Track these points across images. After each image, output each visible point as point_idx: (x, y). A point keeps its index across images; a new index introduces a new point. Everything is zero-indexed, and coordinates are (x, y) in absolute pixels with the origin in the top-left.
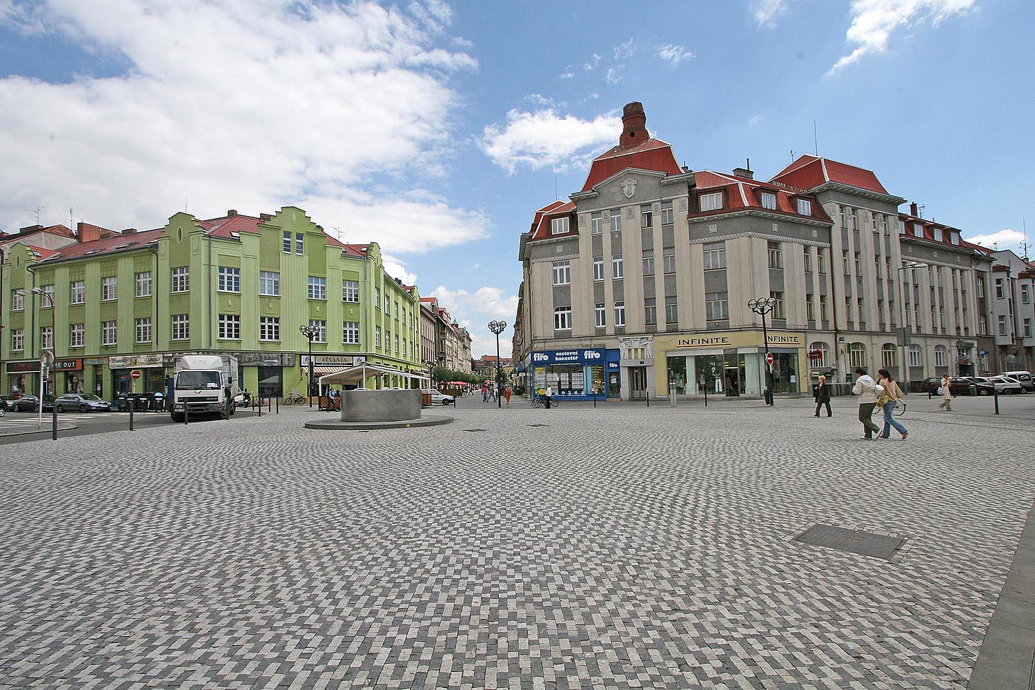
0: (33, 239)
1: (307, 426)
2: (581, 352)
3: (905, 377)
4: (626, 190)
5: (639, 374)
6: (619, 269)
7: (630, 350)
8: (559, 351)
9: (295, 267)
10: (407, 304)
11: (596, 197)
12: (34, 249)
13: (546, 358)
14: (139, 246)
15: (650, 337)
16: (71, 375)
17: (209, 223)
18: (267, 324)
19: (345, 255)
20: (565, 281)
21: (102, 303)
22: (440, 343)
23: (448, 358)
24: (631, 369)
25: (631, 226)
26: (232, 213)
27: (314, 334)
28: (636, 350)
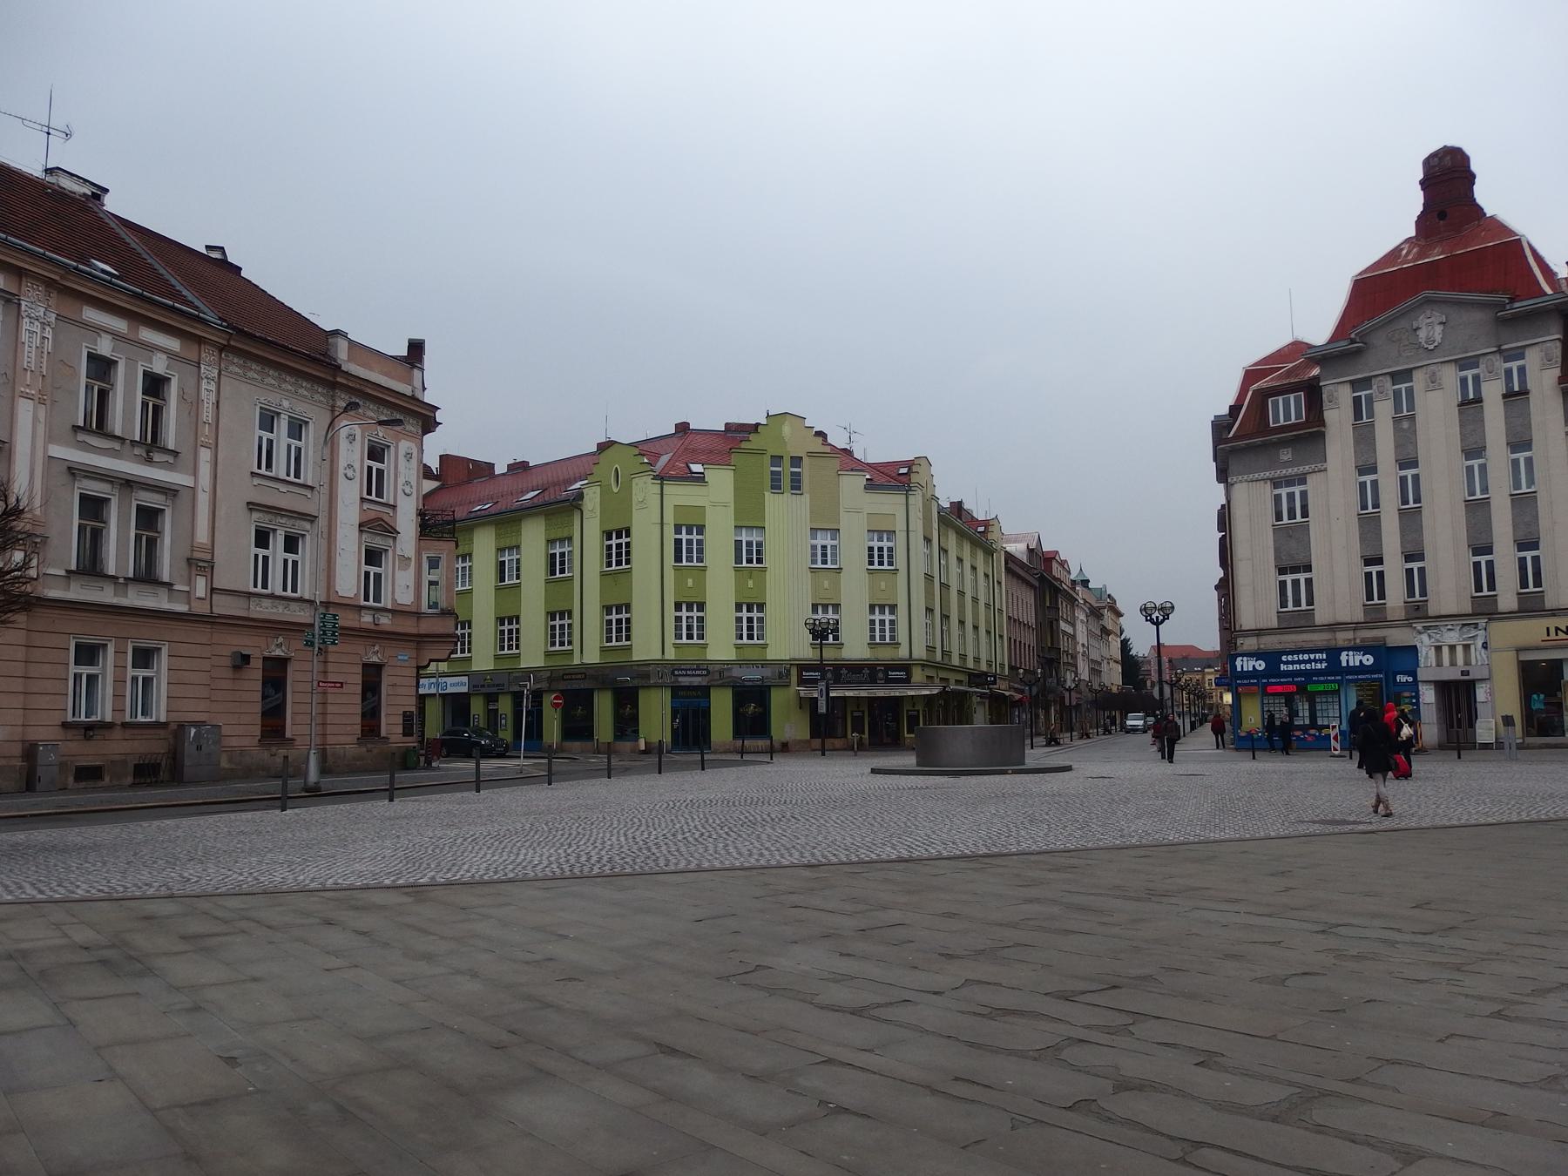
2: (1333, 653)
3: (751, 607)
4: (1422, 334)
5: (1458, 698)
6: (1410, 493)
7: (1438, 649)
8: (1287, 653)
9: (785, 518)
10: (980, 555)
11: (1359, 352)
13: (1261, 665)
15: (1482, 622)
18: (745, 614)
19: (871, 486)
20: (1290, 603)
21: (497, 589)
22: (1048, 625)
23: (1064, 659)
24: (1443, 687)
25: (1436, 407)
26: (683, 428)
28: (1452, 648)
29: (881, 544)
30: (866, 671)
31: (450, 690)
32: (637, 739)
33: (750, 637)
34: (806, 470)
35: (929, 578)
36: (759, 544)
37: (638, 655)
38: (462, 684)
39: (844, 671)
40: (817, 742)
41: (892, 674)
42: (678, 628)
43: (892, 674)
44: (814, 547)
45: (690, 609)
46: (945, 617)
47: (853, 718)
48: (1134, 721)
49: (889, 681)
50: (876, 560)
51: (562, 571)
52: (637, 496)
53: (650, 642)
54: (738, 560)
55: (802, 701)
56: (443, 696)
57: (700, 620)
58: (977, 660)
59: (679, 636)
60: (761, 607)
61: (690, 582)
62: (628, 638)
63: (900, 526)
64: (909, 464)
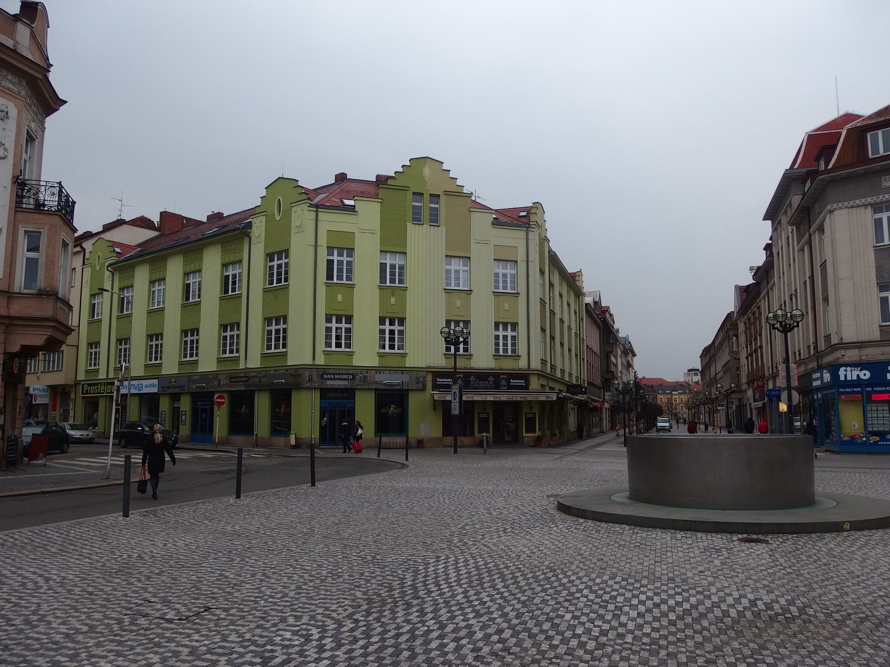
0: (115, 235)
1: (563, 508)
3: (393, 322)
9: (423, 242)
12: (114, 244)
13: (866, 375)
14: (229, 231)
16: (203, 402)
17: (317, 191)
18: (387, 327)
19: (496, 223)
21: (183, 306)
26: (341, 178)
27: (461, 339)
29: (505, 271)
30: (491, 379)
31: (145, 390)
32: (288, 436)
33: (392, 347)
34: (443, 205)
35: (543, 301)
36: (402, 268)
37: (293, 360)
38: (154, 386)
39: (472, 378)
40: (449, 440)
41: (513, 382)
42: (328, 337)
43: (513, 382)
44: (448, 272)
45: (339, 321)
46: (552, 338)
47: (480, 419)
48: (846, 439)
49: (510, 387)
50: (501, 285)
51: (234, 290)
52: (295, 222)
53: (301, 351)
54: (383, 278)
55: (435, 404)
56: (141, 396)
57: (348, 331)
58: (570, 375)
59: (328, 345)
60: (402, 321)
61: (340, 298)
62: (284, 346)
63: (521, 257)
64: (528, 210)
